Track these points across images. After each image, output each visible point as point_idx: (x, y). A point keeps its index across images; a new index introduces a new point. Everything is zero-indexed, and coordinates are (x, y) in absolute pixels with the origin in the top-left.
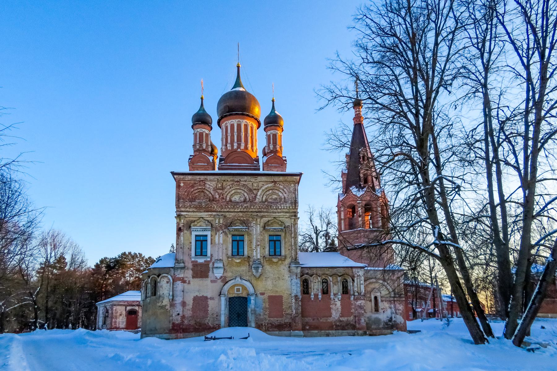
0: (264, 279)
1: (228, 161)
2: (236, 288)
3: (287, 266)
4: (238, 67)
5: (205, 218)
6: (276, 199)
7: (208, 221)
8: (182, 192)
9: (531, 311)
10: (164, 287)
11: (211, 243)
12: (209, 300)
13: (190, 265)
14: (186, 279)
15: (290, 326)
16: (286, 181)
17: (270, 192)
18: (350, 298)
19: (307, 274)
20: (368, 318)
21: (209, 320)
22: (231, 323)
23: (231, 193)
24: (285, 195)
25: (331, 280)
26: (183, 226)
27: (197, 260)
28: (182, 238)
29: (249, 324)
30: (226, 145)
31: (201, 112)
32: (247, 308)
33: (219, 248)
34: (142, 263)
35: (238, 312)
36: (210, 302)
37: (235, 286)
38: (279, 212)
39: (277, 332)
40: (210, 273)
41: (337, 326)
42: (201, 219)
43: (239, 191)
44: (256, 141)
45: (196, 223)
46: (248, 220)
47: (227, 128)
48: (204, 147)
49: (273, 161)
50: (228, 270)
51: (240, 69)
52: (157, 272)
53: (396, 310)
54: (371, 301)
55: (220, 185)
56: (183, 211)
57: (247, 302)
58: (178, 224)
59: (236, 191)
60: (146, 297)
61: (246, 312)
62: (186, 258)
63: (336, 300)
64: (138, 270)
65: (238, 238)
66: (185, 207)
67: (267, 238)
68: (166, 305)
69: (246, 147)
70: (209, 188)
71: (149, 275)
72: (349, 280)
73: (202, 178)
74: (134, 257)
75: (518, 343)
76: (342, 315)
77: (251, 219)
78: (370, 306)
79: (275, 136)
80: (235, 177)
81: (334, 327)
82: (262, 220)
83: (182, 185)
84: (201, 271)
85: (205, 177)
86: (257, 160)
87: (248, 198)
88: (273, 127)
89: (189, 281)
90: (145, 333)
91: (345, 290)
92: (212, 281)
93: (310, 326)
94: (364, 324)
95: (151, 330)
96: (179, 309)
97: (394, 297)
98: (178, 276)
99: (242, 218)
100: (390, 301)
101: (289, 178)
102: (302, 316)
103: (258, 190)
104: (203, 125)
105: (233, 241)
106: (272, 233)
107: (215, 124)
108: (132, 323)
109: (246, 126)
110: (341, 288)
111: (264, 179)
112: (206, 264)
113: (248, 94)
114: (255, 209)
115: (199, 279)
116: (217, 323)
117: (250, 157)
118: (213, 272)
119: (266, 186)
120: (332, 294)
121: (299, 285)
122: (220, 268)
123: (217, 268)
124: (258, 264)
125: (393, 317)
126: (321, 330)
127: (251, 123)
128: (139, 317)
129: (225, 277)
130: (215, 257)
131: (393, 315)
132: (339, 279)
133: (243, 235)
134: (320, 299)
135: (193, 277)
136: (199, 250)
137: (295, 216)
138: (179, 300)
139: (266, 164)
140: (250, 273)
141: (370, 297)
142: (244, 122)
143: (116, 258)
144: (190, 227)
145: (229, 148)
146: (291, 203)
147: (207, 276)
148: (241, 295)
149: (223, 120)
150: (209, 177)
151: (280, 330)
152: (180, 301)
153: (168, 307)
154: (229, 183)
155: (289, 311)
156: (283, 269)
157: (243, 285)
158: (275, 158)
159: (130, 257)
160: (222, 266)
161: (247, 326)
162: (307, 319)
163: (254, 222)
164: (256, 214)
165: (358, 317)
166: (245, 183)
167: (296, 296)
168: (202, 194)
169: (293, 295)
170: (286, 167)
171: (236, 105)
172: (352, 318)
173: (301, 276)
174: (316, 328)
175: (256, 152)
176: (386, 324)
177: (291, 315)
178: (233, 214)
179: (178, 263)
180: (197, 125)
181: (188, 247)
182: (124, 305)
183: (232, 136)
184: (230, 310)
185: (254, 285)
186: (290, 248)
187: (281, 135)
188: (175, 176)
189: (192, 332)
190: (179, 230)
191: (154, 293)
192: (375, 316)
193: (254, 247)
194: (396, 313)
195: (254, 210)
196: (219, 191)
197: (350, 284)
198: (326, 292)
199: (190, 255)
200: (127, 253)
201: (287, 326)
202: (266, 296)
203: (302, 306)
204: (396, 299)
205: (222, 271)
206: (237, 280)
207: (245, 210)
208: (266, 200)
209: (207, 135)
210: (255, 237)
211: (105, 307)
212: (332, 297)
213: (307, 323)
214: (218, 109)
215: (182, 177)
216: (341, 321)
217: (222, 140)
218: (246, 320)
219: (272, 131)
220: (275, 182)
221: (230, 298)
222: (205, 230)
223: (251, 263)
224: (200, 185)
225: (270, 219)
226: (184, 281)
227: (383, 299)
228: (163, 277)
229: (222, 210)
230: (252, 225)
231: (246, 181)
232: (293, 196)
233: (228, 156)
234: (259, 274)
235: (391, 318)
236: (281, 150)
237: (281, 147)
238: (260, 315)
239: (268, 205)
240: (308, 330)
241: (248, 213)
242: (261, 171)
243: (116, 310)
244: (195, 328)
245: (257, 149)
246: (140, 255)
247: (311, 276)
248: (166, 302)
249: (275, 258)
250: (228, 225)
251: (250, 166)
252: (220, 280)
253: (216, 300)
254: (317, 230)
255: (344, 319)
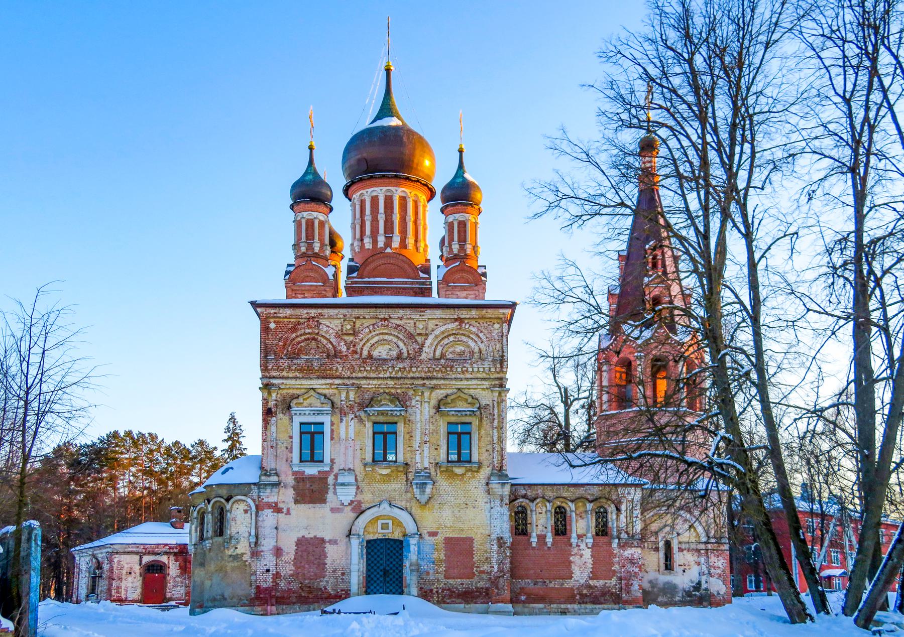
0: (437, 506)
1: (365, 273)
2: (380, 522)
3: (484, 482)
4: (388, 71)
5: (319, 391)
6: (461, 354)
7: (325, 396)
8: (272, 341)
9: (887, 570)
10: (240, 520)
11: (332, 439)
12: (327, 545)
13: (290, 480)
14: (281, 505)
15: (487, 594)
16: (483, 318)
17: (451, 338)
18: (610, 544)
19: (524, 496)
20: (650, 582)
21: (327, 582)
22: (370, 586)
23: (372, 342)
24: (482, 346)
25: (573, 508)
26: (276, 405)
27: (303, 469)
28: (274, 429)
29: (405, 590)
30: (362, 240)
31: (310, 177)
32: (402, 560)
33: (346, 448)
34: (157, 455)
35: (385, 567)
36: (330, 549)
37: (377, 518)
38: (467, 379)
39: (462, 606)
40: (330, 496)
41: (581, 595)
42: (312, 392)
43: (387, 337)
44: (425, 229)
45: (301, 400)
46: (405, 394)
47: (362, 202)
48: (317, 249)
49: (458, 276)
50: (366, 489)
51: (392, 74)
52: (224, 492)
53: (709, 568)
54: (657, 549)
55: (349, 327)
56: (274, 378)
57: (401, 549)
58: (265, 401)
59: (381, 337)
60: (202, 538)
61: (401, 566)
62: (282, 467)
63: (583, 546)
64: (148, 473)
65: (385, 428)
66: (279, 369)
67: (443, 429)
68: (242, 554)
69: (403, 245)
70: (327, 332)
71: (178, 485)
72: (611, 509)
73: (313, 312)
74: (137, 441)
75: (863, 622)
76: (594, 575)
77: (411, 392)
78: (654, 560)
79: (462, 225)
80: (379, 310)
81: (578, 597)
82: (434, 394)
83: (272, 326)
84: (312, 491)
85: (320, 311)
86: (426, 270)
87: (405, 351)
88: (459, 207)
89: (288, 510)
90: (201, 607)
91: (603, 530)
92: (333, 510)
93: (528, 595)
94: (639, 594)
95: (214, 600)
96: (268, 560)
97: (706, 543)
98: (266, 500)
99: (393, 391)
100: (698, 551)
101: (490, 313)
102: (512, 576)
103: (427, 335)
104: (313, 205)
105: (374, 433)
106: (453, 419)
107: (338, 200)
108: (154, 589)
109: (403, 199)
110: (594, 524)
111: (438, 313)
112: (322, 479)
113: (410, 133)
114: (420, 372)
115: (307, 506)
116: (342, 586)
117: (410, 263)
118: (335, 493)
119: (443, 329)
120: (574, 535)
121: (506, 518)
122: (349, 484)
123: (343, 484)
124: (424, 479)
125: (703, 582)
126: (551, 603)
127: (411, 192)
128: (168, 578)
129: (360, 503)
130: (339, 464)
131: (704, 578)
132: (589, 506)
133: (396, 423)
134: (534, 545)
135: (296, 502)
136: (307, 451)
137: (501, 386)
138: (267, 544)
139: (445, 282)
140: (409, 495)
141: (657, 543)
142: (398, 192)
143: (94, 444)
144: (289, 407)
145: (368, 244)
146: (494, 361)
147: (323, 501)
148: (390, 536)
149: (354, 187)
150: (325, 311)
151: (467, 602)
152: (271, 547)
153: (247, 557)
154: (367, 323)
155: (486, 567)
156: (475, 486)
157: (391, 517)
158: (462, 270)
159: (129, 443)
160: (353, 481)
161: (402, 593)
162: (522, 583)
163: (418, 398)
164: (421, 382)
165: (626, 580)
166: (399, 322)
167: (500, 539)
168: (314, 343)
169: (494, 536)
170: (484, 288)
171: (382, 156)
172: (614, 581)
173: (512, 501)
174: (540, 599)
175: (425, 250)
176: (688, 594)
177: (489, 573)
178: (375, 382)
179: (265, 475)
180: (301, 205)
181: (285, 445)
182: (137, 553)
183: (375, 220)
184: (368, 565)
185: (417, 518)
186: (490, 447)
187: (476, 224)
188: (259, 310)
189: (294, 603)
190: (268, 413)
191: (220, 530)
192: (664, 578)
193: (416, 445)
194: (709, 573)
195: (417, 375)
196: (346, 337)
197: (612, 516)
198: (561, 529)
199: (289, 461)
200: (122, 434)
201: (481, 593)
202: (440, 538)
203: (512, 557)
204: (709, 546)
205: (353, 490)
206: (382, 506)
207: (399, 375)
208: (443, 356)
209: (322, 224)
210: (419, 426)
211: (94, 556)
212: (574, 540)
213: (522, 589)
214: (344, 162)
215: (272, 311)
216: (589, 587)
217: (354, 228)
218: (401, 582)
219: (457, 215)
220: (460, 320)
221: (368, 542)
222: (320, 413)
223: (411, 476)
224: (310, 327)
225: (449, 391)
226: (278, 510)
227: (683, 546)
228: (236, 501)
229: (354, 375)
230: (414, 403)
231: (401, 319)
232: (498, 346)
233: (365, 263)
234: (426, 497)
235: (699, 583)
236: (476, 253)
237: (475, 247)
238: (428, 573)
239: (447, 364)
240: (524, 602)
241: (407, 381)
242: (435, 298)
243: (119, 563)
244: (301, 596)
245: (426, 246)
246: (153, 437)
247: (533, 500)
248: (243, 548)
249: (460, 466)
250: (365, 404)
251: (412, 283)
252: (349, 508)
253: (342, 546)
254: (567, 397)
255: (599, 583)
